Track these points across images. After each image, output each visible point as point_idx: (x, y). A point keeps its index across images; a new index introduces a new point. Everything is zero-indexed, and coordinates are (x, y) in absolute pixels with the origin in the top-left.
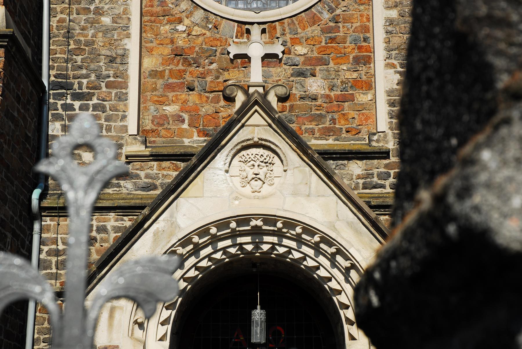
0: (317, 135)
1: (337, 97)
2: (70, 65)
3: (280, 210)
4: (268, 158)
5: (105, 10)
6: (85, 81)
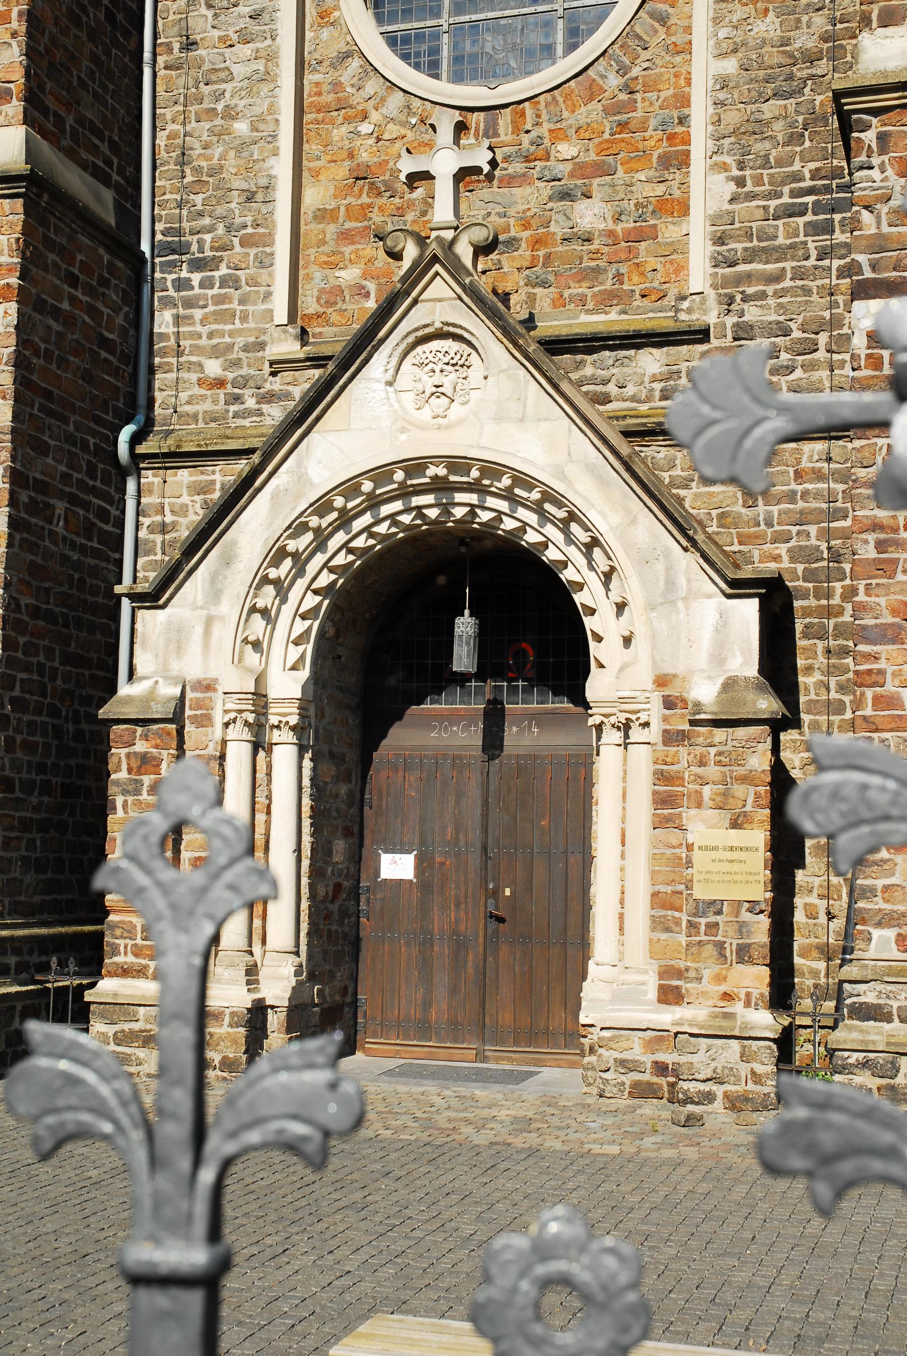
0: (590, 305)
1: (627, 232)
2: (185, 212)
3: (473, 447)
4: (458, 356)
5: (239, 109)
6: (208, 237)
